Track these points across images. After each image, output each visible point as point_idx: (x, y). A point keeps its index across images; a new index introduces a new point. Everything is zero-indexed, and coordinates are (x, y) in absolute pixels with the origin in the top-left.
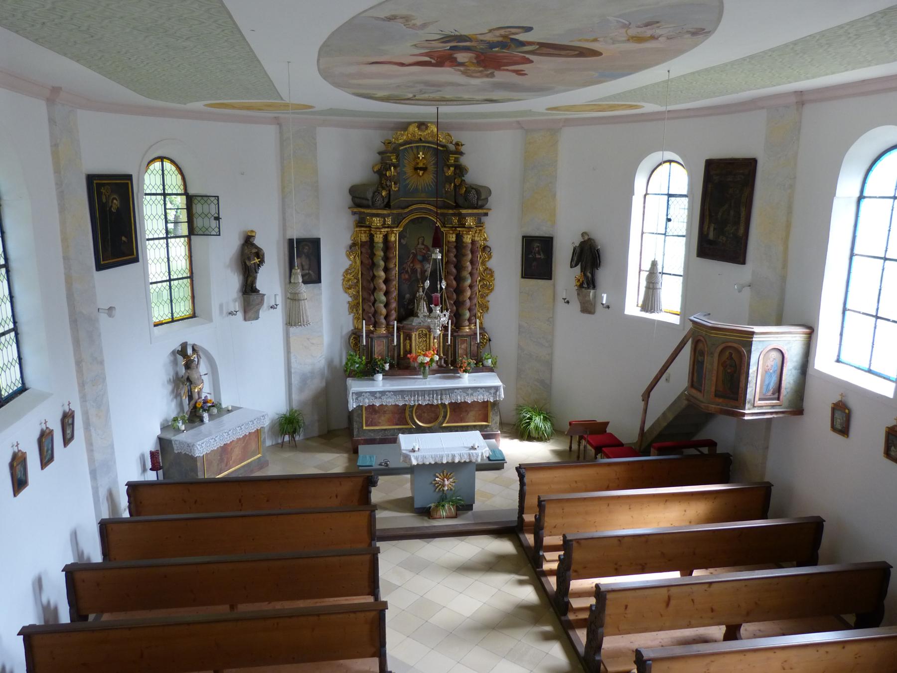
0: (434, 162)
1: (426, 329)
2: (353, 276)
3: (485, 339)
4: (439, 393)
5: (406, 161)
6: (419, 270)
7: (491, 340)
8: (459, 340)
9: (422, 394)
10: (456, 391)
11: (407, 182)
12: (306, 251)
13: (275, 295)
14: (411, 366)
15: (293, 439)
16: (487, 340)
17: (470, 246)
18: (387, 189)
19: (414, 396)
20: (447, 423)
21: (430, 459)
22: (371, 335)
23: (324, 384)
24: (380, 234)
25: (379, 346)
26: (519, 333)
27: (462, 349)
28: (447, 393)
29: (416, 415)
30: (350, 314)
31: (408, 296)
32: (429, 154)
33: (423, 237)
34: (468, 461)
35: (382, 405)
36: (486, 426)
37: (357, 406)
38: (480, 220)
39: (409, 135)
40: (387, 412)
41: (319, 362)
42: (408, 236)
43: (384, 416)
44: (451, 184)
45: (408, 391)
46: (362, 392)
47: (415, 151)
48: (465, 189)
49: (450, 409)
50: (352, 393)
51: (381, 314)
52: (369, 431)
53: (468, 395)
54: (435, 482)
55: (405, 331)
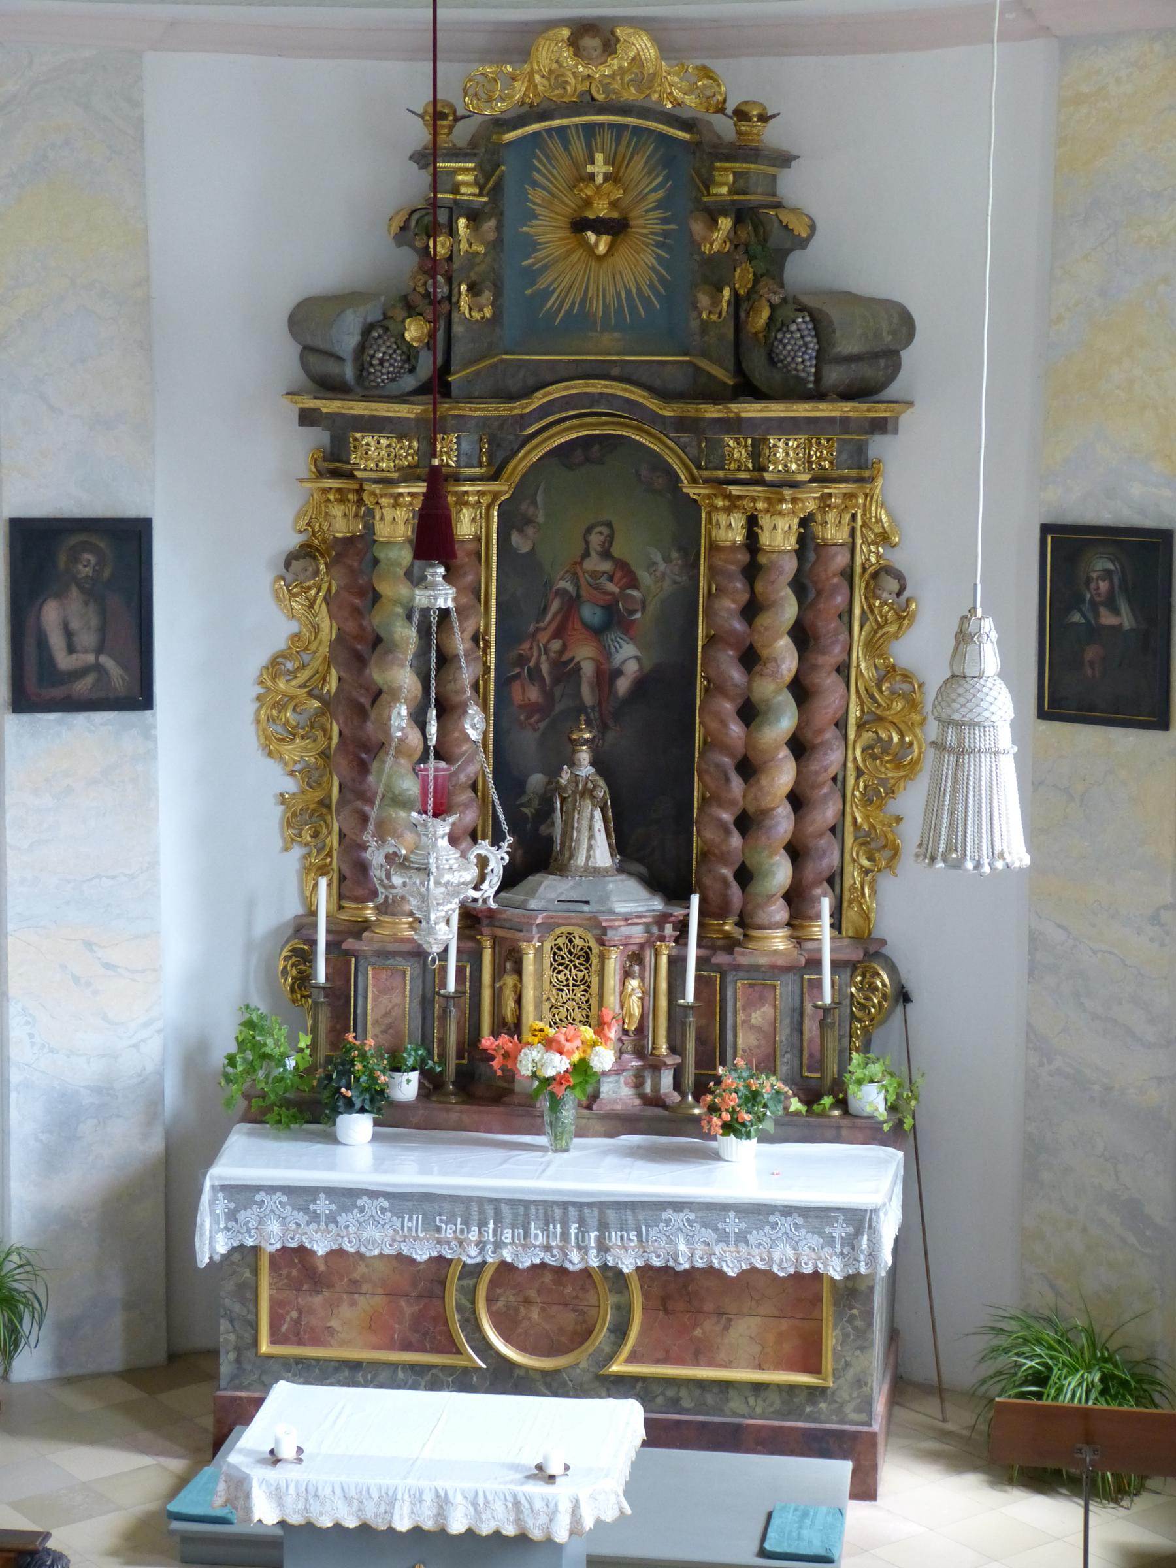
0: (661, 193)
1: (587, 928)
3: (874, 989)
5: (540, 192)
6: (588, 669)
7: (914, 995)
8: (737, 990)
9: (515, 1216)
10: (668, 1214)
11: (542, 284)
12: (84, 571)
16: (884, 996)
17: (790, 566)
19: (482, 1224)
20: (633, 1358)
22: (350, 944)
23: (155, 1145)
25: (383, 991)
26: (1031, 974)
27: (752, 1027)
28: (630, 1220)
32: (639, 162)
33: (609, 525)
34: (510, 1530)
35: (340, 1252)
36: (814, 1393)
37: (233, 1250)
38: (860, 450)
39: (537, 78)
40: (365, 1288)
41: (136, 1046)
42: (541, 519)
43: (353, 1304)
44: (721, 290)
45: (455, 1199)
47: (578, 147)
48: (766, 313)
49: (646, 1296)
50: (213, 1187)
53: (723, 1237)
55: (500, 933)
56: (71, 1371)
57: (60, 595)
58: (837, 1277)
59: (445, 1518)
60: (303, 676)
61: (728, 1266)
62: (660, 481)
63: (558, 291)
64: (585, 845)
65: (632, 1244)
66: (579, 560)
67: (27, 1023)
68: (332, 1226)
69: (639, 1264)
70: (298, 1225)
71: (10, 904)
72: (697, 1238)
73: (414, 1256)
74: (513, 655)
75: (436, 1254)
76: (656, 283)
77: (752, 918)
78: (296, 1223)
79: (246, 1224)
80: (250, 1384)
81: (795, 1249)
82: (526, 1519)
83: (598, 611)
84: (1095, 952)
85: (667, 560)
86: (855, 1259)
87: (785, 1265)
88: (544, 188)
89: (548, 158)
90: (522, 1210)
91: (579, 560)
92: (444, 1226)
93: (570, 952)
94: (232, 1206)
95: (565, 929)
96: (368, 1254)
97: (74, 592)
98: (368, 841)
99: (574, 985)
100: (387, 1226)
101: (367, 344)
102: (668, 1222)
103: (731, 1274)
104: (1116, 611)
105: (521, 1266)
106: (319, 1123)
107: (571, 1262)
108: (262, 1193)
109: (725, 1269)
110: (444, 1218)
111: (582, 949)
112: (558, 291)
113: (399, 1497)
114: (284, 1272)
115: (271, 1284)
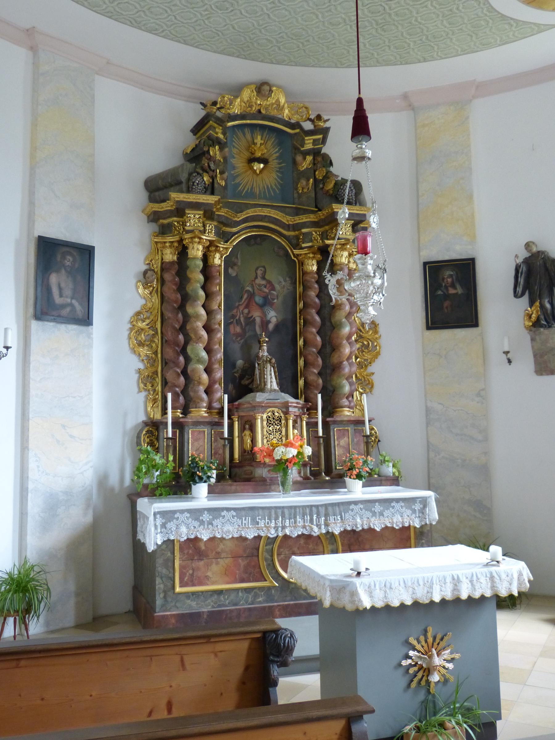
0: (277, 154)
2: (147, 325)
4: (322, 511)
6: (258, 320)
8: (335, 430)
9: (290, 514)
10: (352, 507)
11: (237, 181)
13: (6, 330)
14: (256, 475)
15: (23, 626)
18: (211, 173)
19: (276, 519)
21: (402, 590)
23: (89, 519)
24: (199, 243)
25: (195, 440)
27: (341, 446)
29: (278, 561)
30: (140, 391)
31: (240, 363)
32: (270, 143)
33: (264, 267)
37: (164, 542)
40: (223, 555)
41: (82, 473)
42: (239, 264)
43: (217, 563)
44: (309, 180)
45: (263, 508)
46: (174, 512)
50: (155, 514)
51: (200, 383)
52: (188, 595)
53: (374, 514)
54: (409, 661)
56: (52, 628)
57: (58, 271)
58: (418, 527)
59: (459, 591)
60: (148, 321)
61: (377, 527)
62: (282, 253)
63: (243, 184)
64: (269, 381)
65: (339, 521)
66: (254, 280)
67: (37, 461)
68: (210, 526)
69: (342, 530)
70: (195, 527)
71: (31, 405)
72: (364, 516)
73: (247, 536)
74: (230, 314)
75: (256, 535)
76: (277, 185)
77: (338, 404)
78: (194, 526)
79: (170, 529)
80: (171, 608)
81: (401, 517)
82: (498, 585)
83: (261, 299)
84: (455, 411)
85: (285, 281)
86: (425, 518)
87: (398, 524)
88: (237, 148)
89: (237, 137)
90: (293, 511)
91: (254, 280)
92: (260, 521)
93: (274, 419)
94: (164, 521)
95: (273, 409)
96: (227, 538)
97: (63, 271)
98: (326, 275)
99: (276, 432)
100: (235, 524)
101: (191, 178)
102: (352, 510)
103: (378, 530)
104: (455, 288)
105: (293, 536)
106: (177, 495)
107: (314, 532)
108: (178, 514)
109: (376, 528)
110: (260, 517)
111: (278, 417)
112: (243, 184)
113: (434, 582)
114: (186, 552)
115: (180, 558)
